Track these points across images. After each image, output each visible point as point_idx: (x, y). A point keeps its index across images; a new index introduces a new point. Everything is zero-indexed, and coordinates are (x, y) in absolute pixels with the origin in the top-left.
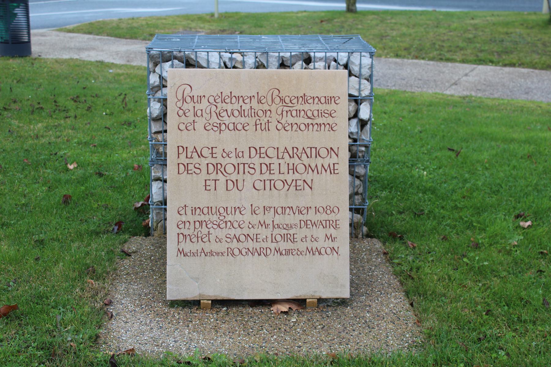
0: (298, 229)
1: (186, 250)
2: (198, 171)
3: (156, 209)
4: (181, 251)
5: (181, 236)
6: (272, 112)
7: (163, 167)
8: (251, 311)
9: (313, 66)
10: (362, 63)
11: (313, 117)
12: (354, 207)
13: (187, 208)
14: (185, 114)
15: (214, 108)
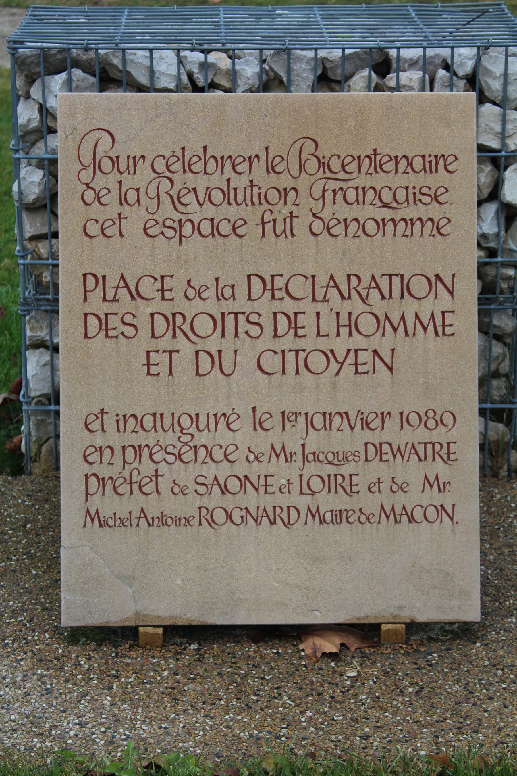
0: (360, 463)
1: (106, 513)
2: (130, 331)
3: (35, 412)
4: (93, 515)
5: (93, 480)
6: (300, 193)
7: (52, 317)
8: (255, 652)
9: (395, 79)
10: (509, 72)
11: (395, 205)
12: (489, 405)
13: (105, 416)
14: (98, 198)
15: (165, 185)
